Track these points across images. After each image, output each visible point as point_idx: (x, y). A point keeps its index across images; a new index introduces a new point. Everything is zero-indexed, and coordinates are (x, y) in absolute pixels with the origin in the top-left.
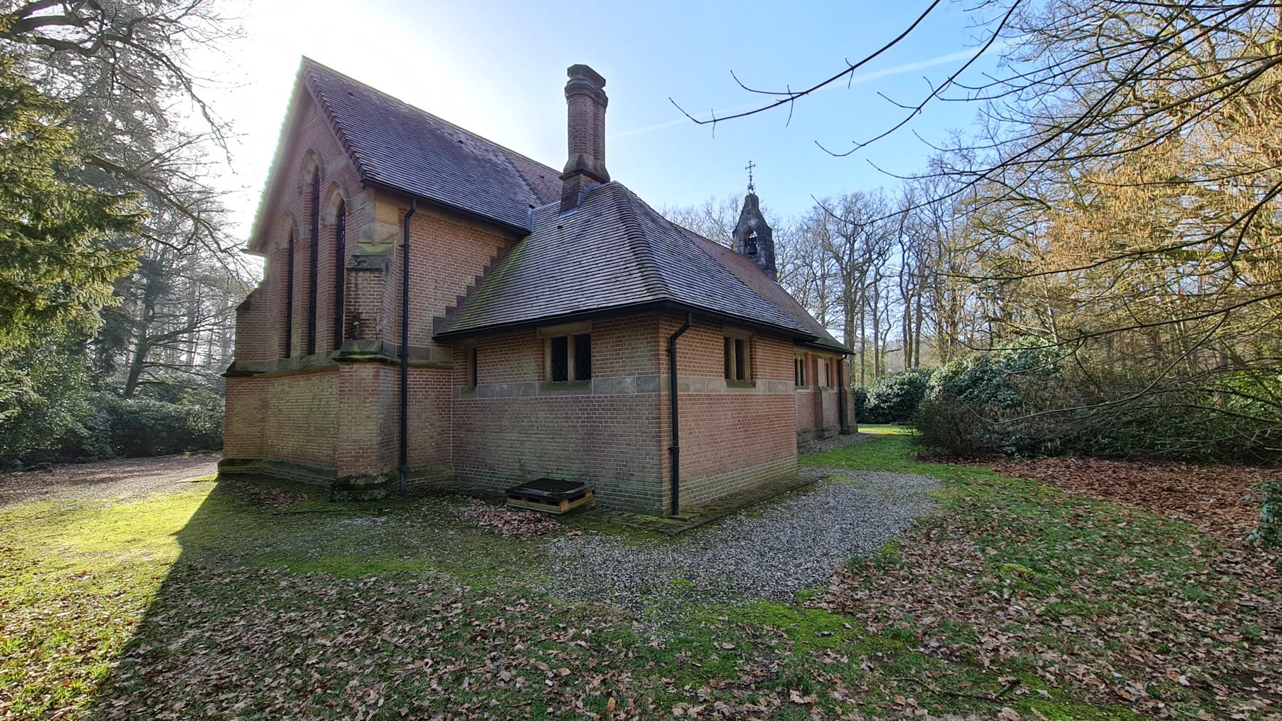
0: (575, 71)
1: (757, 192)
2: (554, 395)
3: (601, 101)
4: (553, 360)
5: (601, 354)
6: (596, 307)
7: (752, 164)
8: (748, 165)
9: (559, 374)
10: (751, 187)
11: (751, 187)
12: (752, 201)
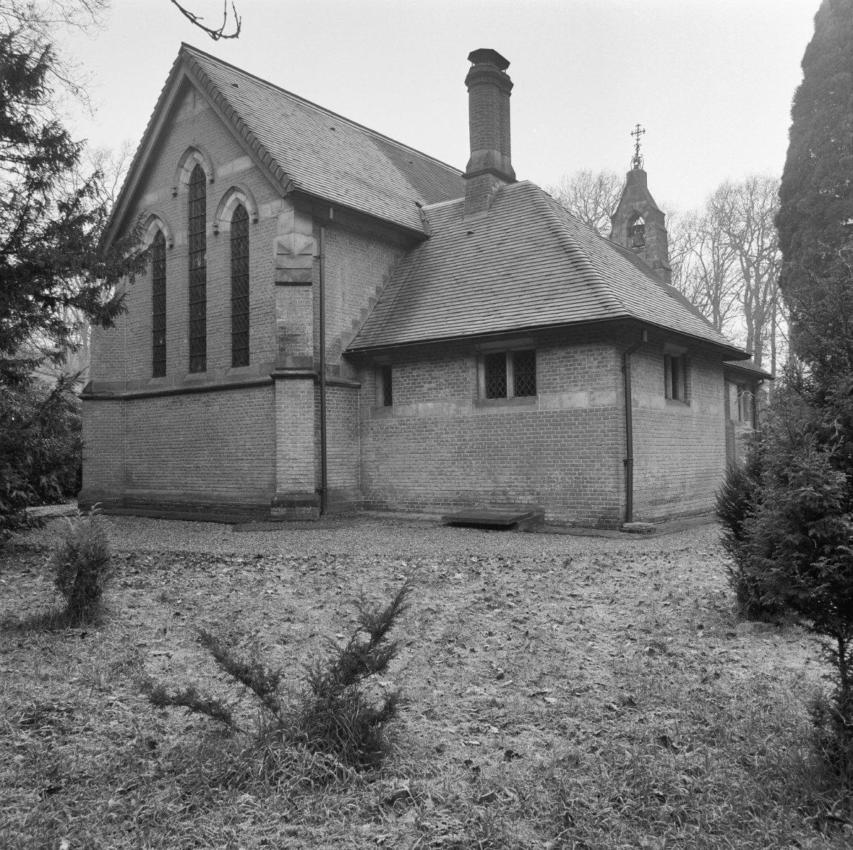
0: (477, 56)
1: (646, 166)
2: (493, 411)
3: (506, 85)
4: (486, 378)
5: (544, 369)
6: (582, 319)
7: (641, 128)
8: (635, 129)
9: (496, 391)
10: (637, 160)
11: (637, 160)
12: (637, 178)
